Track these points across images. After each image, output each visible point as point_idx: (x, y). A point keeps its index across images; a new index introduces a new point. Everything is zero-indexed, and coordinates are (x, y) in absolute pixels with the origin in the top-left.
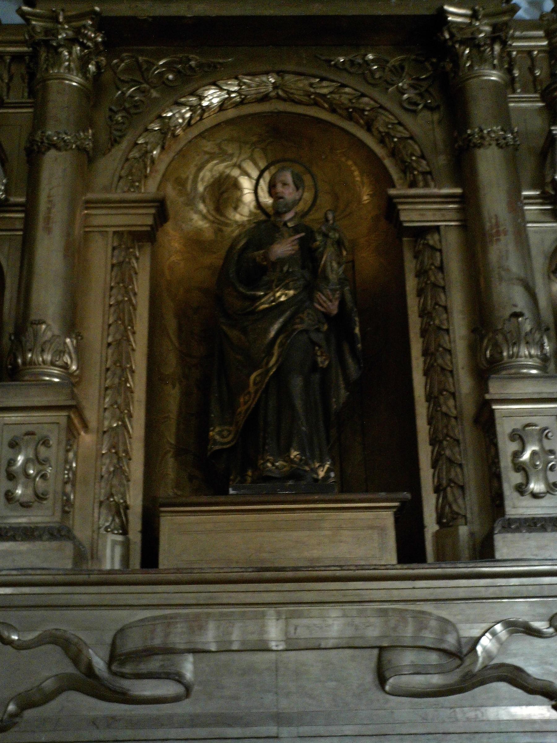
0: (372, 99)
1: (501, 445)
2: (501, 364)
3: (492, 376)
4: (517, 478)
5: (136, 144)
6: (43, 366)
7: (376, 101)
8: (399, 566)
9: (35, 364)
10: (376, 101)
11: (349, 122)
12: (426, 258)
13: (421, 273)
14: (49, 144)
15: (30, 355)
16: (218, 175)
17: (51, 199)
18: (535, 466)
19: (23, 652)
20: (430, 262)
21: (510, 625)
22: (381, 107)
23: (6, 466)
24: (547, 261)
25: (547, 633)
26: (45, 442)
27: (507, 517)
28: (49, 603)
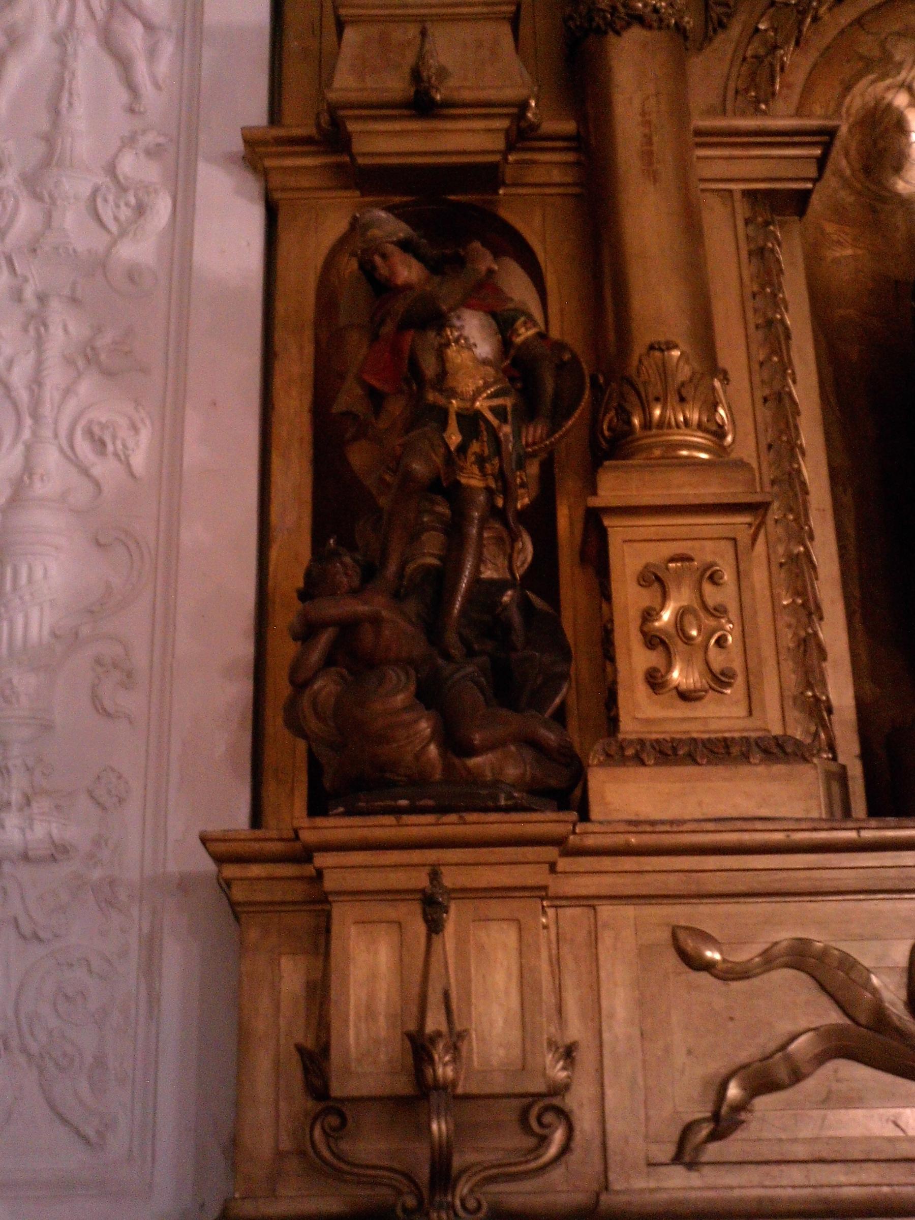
2: (633, 441)
3: (607, 463)
5: (757, 30)
6: (683, 430)
8: (873, 823)
9: (669, 426)
14: (628, 15)
15: (657, 412)
16: (872, 104)
17: (647, 118)
18: (688, 639)
19: (736, 985)
23: (639, 622)
26: (714, 579)
27: (621, 736)
28: (776, 886)
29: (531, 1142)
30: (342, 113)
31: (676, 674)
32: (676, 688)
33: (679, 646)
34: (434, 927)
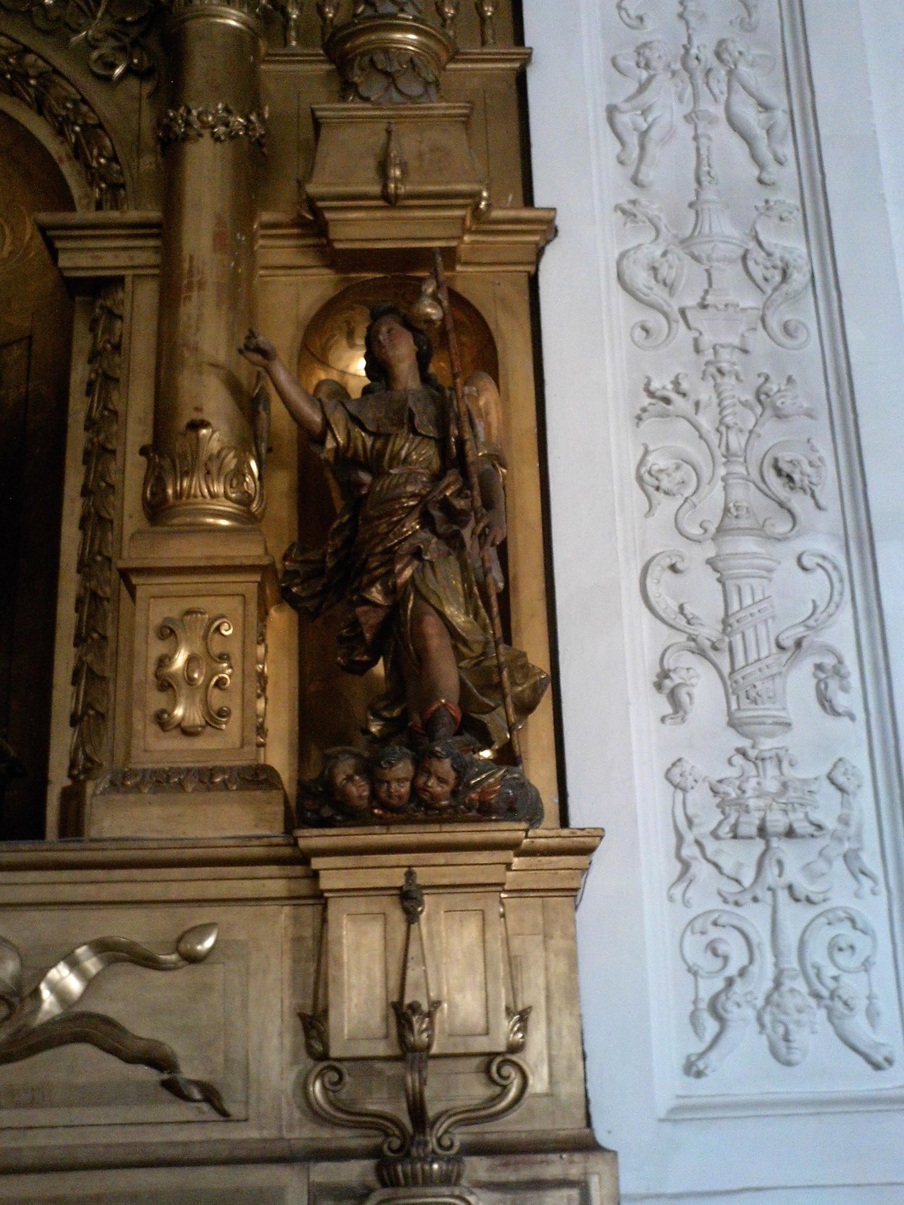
0: (40, 57)
1: (139, 644)
4: (156, 700)
7: (46, 61)
10: (46, 61)
11: (9, 99)
12: (101, 328)
13: (94, 356)
18: (190, 681)
20: (106, 337)
21: (101, 947)
22: (56, 71)
24: (301, 334)
25: (165, 962)
29: (498, 1090)
30: (320, 204)
31: (179, 712)
32: (179, 725)
33: (184, 690)
34: (411, 917)
